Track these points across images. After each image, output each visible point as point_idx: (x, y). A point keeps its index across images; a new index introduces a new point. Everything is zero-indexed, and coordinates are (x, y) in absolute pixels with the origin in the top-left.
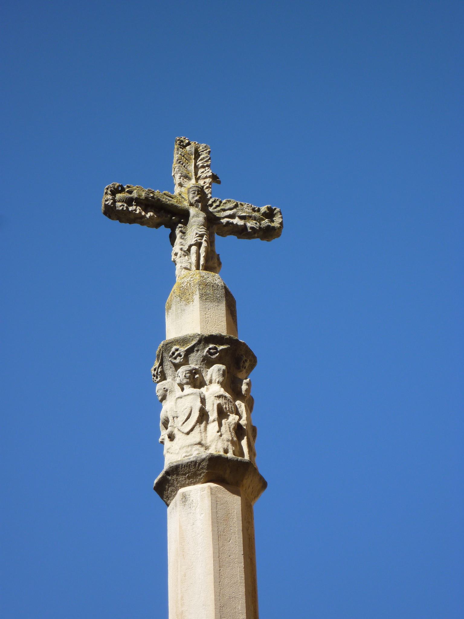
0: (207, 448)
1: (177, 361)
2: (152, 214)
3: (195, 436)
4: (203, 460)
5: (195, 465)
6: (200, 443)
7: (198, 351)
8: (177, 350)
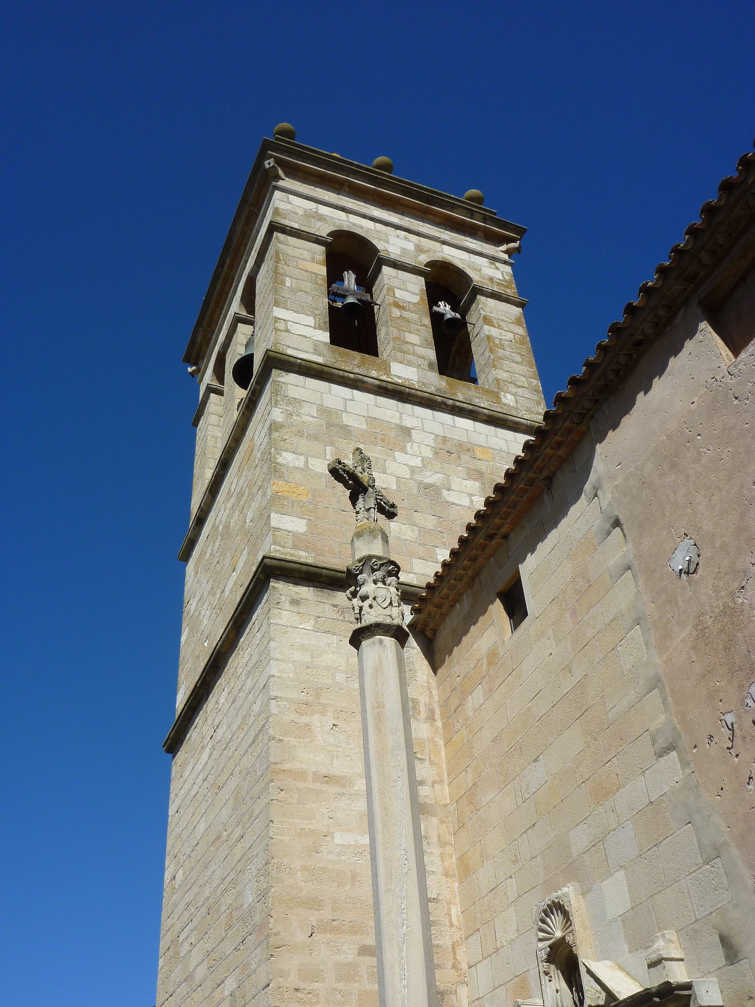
0: (393, 620)
1: (375, 567)
2: (352, 482)
3: (387, 612)
4: (395, 625)
5: (389, 626)
6: (390, 616)
7: (386, 566)
8: (376, 562)
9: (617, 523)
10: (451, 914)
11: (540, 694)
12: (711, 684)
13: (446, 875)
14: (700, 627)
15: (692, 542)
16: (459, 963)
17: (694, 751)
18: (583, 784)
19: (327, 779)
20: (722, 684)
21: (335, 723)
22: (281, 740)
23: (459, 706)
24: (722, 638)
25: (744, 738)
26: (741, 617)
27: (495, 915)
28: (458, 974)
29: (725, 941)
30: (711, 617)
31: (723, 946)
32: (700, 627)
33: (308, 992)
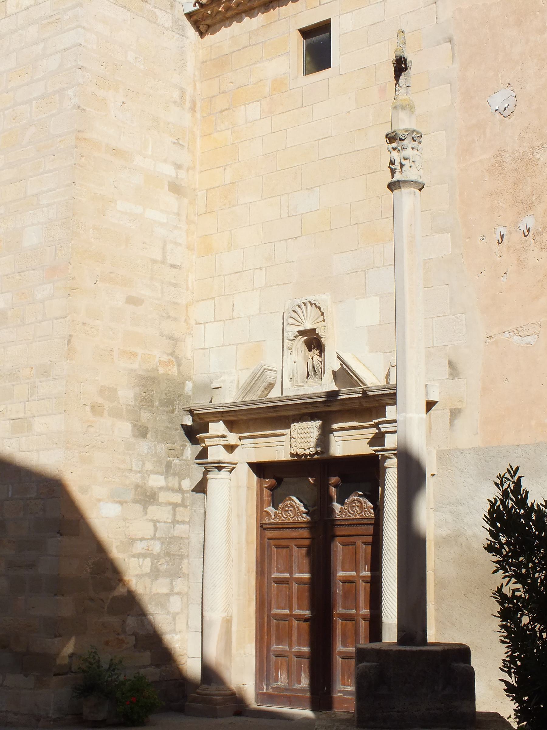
9: (450, 40)
10: (188, 280)
11: (328, 139)
12: (495, 202)
13: (188, 248)
14: (499, 159)
15: (514, 94)
16: (189, 318)
17: (467, 240)
18: (356, 225)
19: (116, 152)
20: (504, 206)
21: (125, 101)
22: (84, 110)
23: (227, 109)
24: (514, 175)
25: (509, 247)
26: (534, 168)
27: (235, 292)
28: (188, 327)
29: (450, 363)
30: (510, 156)
31: (449, 367)
32: (499, 159)
33: (91, 326)
